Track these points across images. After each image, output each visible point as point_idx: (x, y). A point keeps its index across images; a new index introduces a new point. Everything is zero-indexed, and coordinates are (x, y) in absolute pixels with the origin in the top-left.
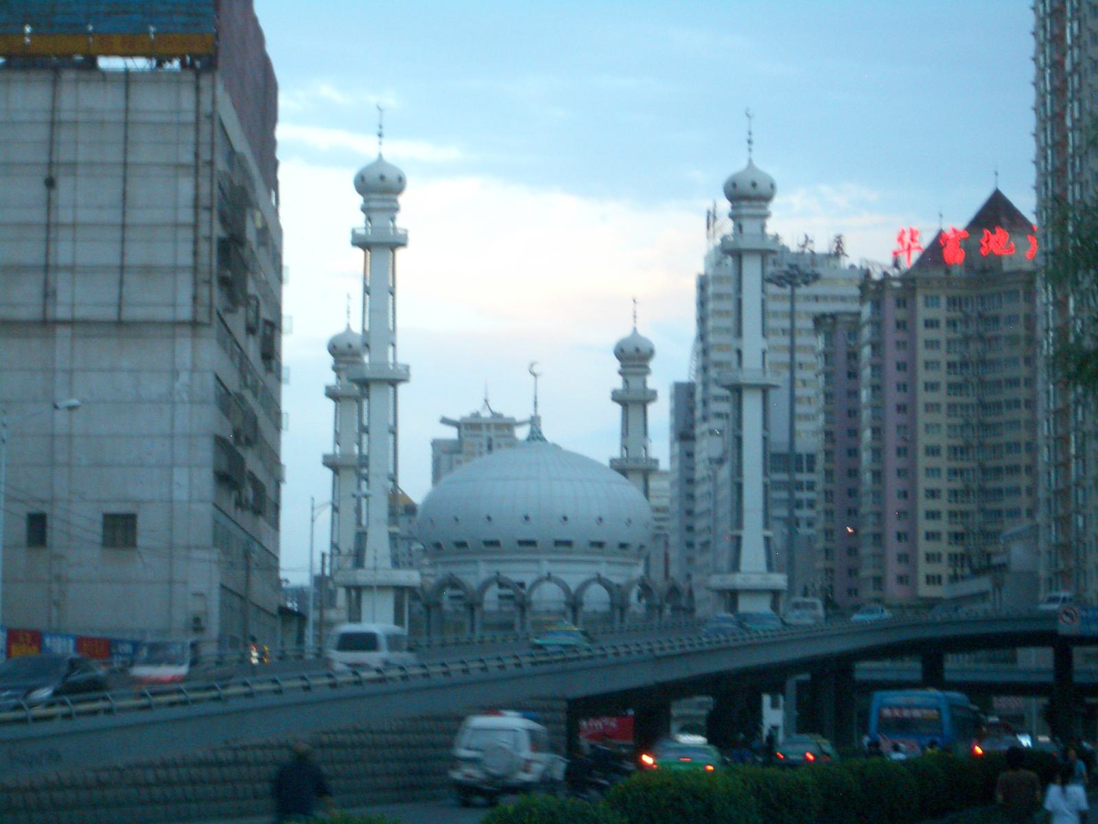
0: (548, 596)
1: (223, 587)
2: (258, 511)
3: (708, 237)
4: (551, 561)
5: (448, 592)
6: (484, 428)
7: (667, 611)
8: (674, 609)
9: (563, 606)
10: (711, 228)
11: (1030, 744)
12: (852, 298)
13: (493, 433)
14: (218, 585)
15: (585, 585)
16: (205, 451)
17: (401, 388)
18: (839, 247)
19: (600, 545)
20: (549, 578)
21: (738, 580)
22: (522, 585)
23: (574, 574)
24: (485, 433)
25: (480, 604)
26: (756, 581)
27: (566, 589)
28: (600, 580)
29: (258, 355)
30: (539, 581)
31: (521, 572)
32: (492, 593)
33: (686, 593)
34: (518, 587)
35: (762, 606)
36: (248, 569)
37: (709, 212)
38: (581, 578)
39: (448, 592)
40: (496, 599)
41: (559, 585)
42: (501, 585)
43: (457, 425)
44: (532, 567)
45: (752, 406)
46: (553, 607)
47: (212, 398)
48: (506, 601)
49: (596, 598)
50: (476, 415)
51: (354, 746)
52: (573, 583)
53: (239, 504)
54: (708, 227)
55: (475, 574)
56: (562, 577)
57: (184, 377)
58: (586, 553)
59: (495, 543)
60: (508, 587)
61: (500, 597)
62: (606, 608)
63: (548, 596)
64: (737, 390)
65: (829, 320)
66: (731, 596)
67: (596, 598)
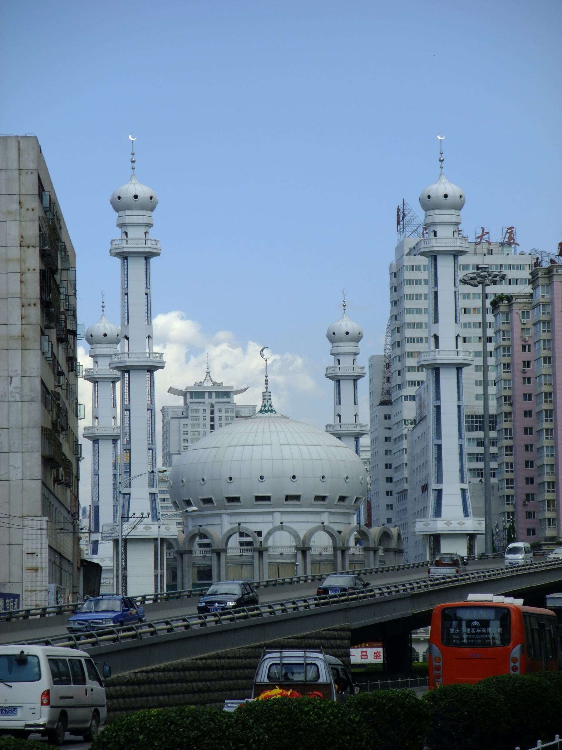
0: (282, 543)
1: (50, 546)
2: (68, 485)
3: (398, 231)
4: (282, 513)
5: (198, 540)
6: (207, 395)
7: (381, 552)
8: (386, 550)
9: (294, 550)
10: (401, 223)
11: (226, 709)
12: (524, 281)
13: (214, 400)
14: (47, 547)
15: (311, 534)
16: (35, 440)
17: (157, 373)
18: (510, 238)
19: (323, 498)
20: (282, 527)
21: (440, 526)
22: (259, 533)
23: (302, 524)
24: (207, 400)
25: (225, 551)
26: (455, 527)
27: (296, 536)
28: (324, 528)
29: (64, 360)
30: (275, 529)
31: (256, 523)
32: (235, 541)
33: (395, 537)
34: (256, 535)
35: (460, 549)
36: (41, 529)
37: (399, 210)
38: (310, 526)
39: (198, 540)
40: (238, 545)
41: (291, 534)
42: (242, 535)
43: (184, 394)
44: (268, 518)
45: (448, 380)
46: (286, 551)
47: (39, 398)
48: (245, 547)
49: (321, 542)
50: (200, 385)
51: (217, 668)
52: (302, 530)
53: (57, 481)
54: (398, 223)
55: (220, 526)
56: (293, 526)
57: (16, 381)
58: (313, 506)
59: (236, 499)
60: (248, 536)
61: (242, 544)
62: (330, 551)
63: (282, 543)
64: (436, 370)
65: (506, 302)
66: (435, 539)
67: (321, 542)
